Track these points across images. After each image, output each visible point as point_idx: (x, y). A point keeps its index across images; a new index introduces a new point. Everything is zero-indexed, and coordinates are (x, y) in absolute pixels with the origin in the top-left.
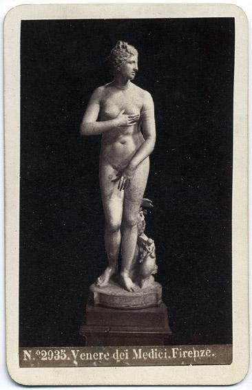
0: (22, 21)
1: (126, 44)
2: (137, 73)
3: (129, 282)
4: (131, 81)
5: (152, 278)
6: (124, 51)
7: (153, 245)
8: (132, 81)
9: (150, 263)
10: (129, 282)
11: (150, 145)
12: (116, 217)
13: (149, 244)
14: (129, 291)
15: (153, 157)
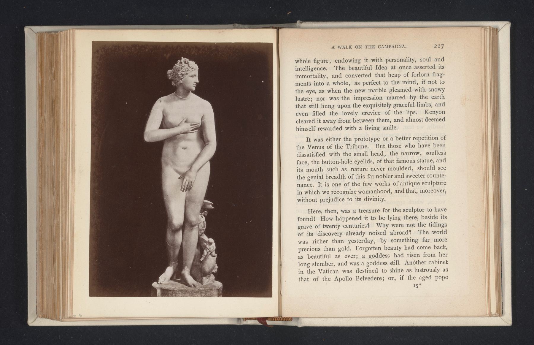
0: (90, 296)
1: (187, 60)
2: (198, 85)
3: (190, 279)
4: (192, 92)
5: (212, 277)
6: (186, 66)
7: (214, 245)
8: (194, 92)
9: (211, 263)
10: (190, 279)
11: (211, 149)
12: (177, 219)
13: (210, 244)
14: (191, 287)
15: (213, 161)
